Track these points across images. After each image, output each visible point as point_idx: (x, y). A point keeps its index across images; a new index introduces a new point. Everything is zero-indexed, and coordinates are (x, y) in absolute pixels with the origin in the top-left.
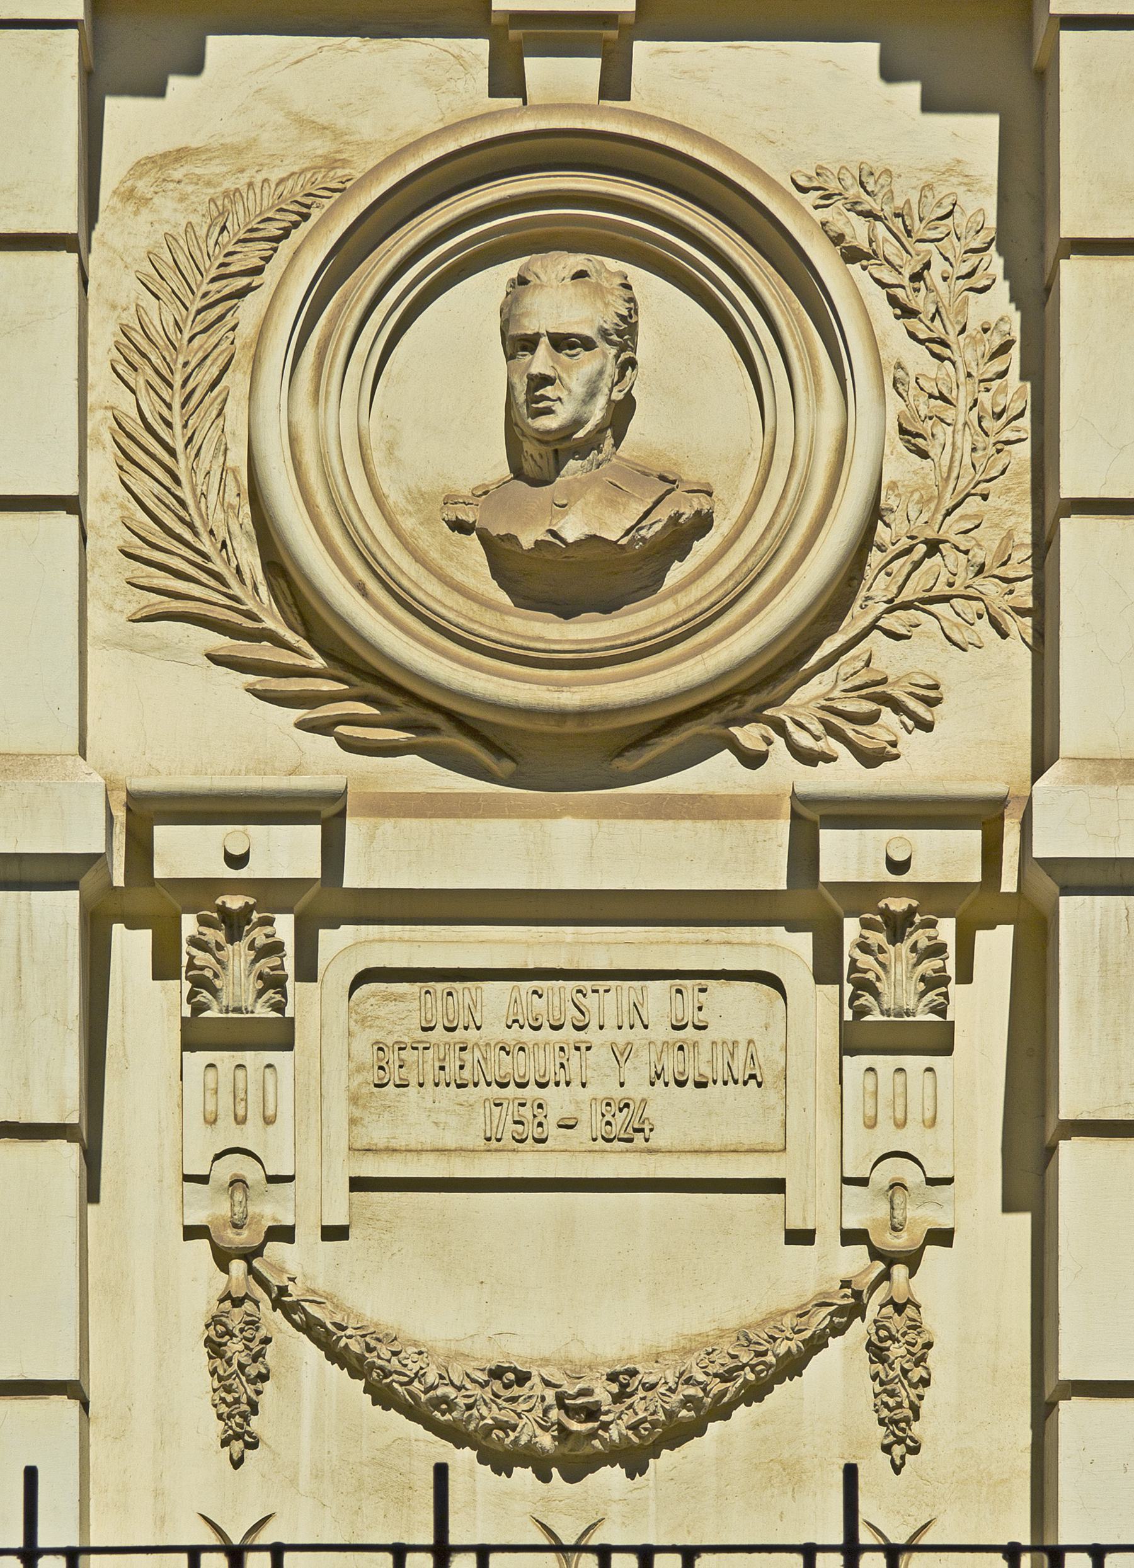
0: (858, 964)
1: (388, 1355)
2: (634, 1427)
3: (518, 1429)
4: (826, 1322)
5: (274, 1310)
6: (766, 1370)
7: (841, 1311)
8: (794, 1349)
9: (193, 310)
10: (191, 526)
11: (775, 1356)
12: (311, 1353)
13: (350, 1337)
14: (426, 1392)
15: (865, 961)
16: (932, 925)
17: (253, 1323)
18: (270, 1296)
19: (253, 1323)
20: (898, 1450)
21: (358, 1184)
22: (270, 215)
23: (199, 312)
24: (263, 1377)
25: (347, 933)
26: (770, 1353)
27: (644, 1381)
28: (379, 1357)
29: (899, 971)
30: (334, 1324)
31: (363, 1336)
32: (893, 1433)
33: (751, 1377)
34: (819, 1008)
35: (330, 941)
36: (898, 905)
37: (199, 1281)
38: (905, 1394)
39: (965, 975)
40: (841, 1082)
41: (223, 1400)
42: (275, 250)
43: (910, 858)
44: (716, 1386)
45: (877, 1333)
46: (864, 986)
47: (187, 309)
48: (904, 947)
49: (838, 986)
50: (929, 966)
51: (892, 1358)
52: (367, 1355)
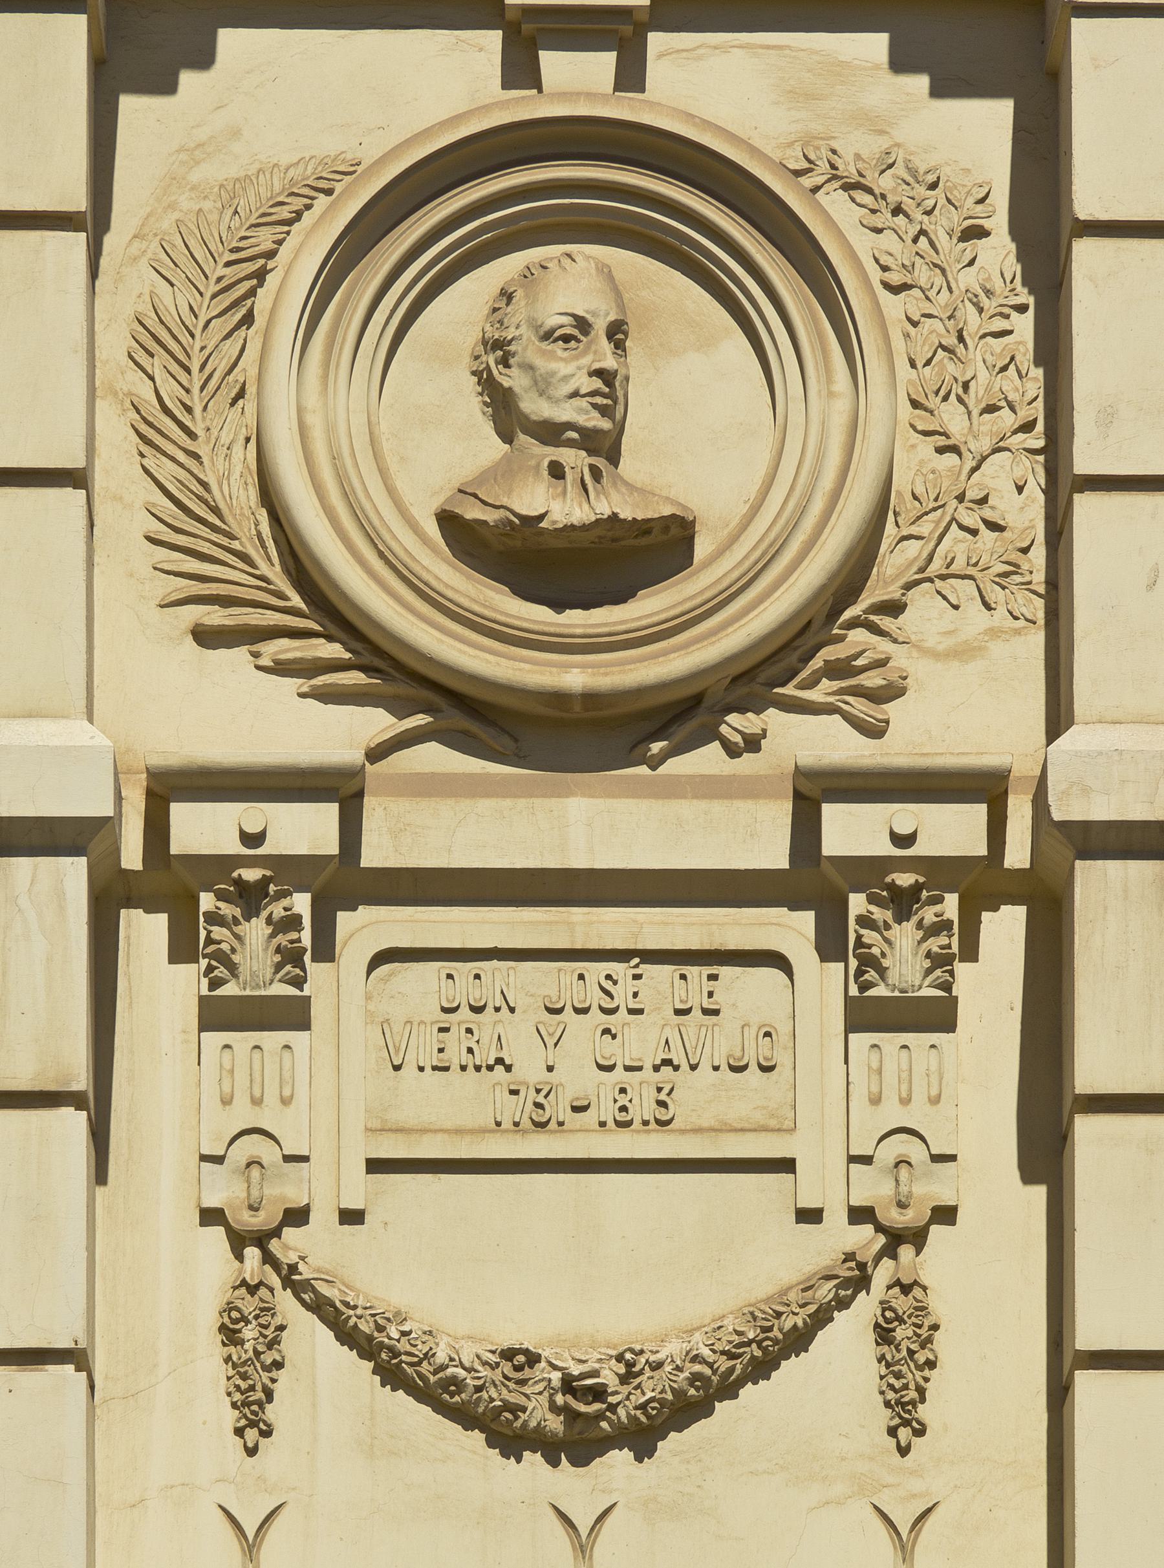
0: (864, 940)
1: (396, 1335)
2: (643, 1407)
3: (528, 1413)
4: (831, 1295)
5: (285, 1289)
6: (769, 1346)
7: (846, 1283)
8: (800, 1324)
9: (208, 295)
10: (216, 510)
11: (781, 1330)
12: (325, 1335)
13: (360, 1317)
14: (435, 1373)
15: (869, 936)
16: (939, 900)
17: (268, 1309)
18: (279, 1275)
19: (267, 1310)
20: (904, 1433)
21: (375, 1166)
22: (280, 199)
23: (214, 296)
24: (278, 1365)
25: (365, 913)
26: (775, 1329)
27: (651, 1359)
28: (390, 1338)
29: (904, 942)
30: (342, 1302)
31: (374, 1315)
32: (901, 1417)
33: (758, 1353)
34: (825, 986)
35: (345, 921)
36: (905, 880)
37: (212, 1263)
38: (912, 1376)
39: (970, 952)
40: (846, 1062)
41: (238, 1387)
42: (288, 233)
43: (916, 831)
44: (724, 1364)
45: (883, 1315)
46: (868, 962)
47: (201, 294)
48: (909, 926)
49: (842, 964)
50: (934, 944)
51: (899, 1338)
52: (376, 1334)
